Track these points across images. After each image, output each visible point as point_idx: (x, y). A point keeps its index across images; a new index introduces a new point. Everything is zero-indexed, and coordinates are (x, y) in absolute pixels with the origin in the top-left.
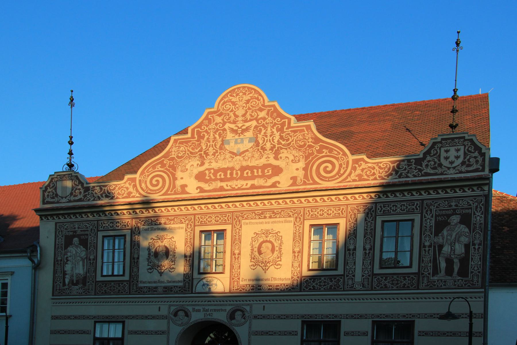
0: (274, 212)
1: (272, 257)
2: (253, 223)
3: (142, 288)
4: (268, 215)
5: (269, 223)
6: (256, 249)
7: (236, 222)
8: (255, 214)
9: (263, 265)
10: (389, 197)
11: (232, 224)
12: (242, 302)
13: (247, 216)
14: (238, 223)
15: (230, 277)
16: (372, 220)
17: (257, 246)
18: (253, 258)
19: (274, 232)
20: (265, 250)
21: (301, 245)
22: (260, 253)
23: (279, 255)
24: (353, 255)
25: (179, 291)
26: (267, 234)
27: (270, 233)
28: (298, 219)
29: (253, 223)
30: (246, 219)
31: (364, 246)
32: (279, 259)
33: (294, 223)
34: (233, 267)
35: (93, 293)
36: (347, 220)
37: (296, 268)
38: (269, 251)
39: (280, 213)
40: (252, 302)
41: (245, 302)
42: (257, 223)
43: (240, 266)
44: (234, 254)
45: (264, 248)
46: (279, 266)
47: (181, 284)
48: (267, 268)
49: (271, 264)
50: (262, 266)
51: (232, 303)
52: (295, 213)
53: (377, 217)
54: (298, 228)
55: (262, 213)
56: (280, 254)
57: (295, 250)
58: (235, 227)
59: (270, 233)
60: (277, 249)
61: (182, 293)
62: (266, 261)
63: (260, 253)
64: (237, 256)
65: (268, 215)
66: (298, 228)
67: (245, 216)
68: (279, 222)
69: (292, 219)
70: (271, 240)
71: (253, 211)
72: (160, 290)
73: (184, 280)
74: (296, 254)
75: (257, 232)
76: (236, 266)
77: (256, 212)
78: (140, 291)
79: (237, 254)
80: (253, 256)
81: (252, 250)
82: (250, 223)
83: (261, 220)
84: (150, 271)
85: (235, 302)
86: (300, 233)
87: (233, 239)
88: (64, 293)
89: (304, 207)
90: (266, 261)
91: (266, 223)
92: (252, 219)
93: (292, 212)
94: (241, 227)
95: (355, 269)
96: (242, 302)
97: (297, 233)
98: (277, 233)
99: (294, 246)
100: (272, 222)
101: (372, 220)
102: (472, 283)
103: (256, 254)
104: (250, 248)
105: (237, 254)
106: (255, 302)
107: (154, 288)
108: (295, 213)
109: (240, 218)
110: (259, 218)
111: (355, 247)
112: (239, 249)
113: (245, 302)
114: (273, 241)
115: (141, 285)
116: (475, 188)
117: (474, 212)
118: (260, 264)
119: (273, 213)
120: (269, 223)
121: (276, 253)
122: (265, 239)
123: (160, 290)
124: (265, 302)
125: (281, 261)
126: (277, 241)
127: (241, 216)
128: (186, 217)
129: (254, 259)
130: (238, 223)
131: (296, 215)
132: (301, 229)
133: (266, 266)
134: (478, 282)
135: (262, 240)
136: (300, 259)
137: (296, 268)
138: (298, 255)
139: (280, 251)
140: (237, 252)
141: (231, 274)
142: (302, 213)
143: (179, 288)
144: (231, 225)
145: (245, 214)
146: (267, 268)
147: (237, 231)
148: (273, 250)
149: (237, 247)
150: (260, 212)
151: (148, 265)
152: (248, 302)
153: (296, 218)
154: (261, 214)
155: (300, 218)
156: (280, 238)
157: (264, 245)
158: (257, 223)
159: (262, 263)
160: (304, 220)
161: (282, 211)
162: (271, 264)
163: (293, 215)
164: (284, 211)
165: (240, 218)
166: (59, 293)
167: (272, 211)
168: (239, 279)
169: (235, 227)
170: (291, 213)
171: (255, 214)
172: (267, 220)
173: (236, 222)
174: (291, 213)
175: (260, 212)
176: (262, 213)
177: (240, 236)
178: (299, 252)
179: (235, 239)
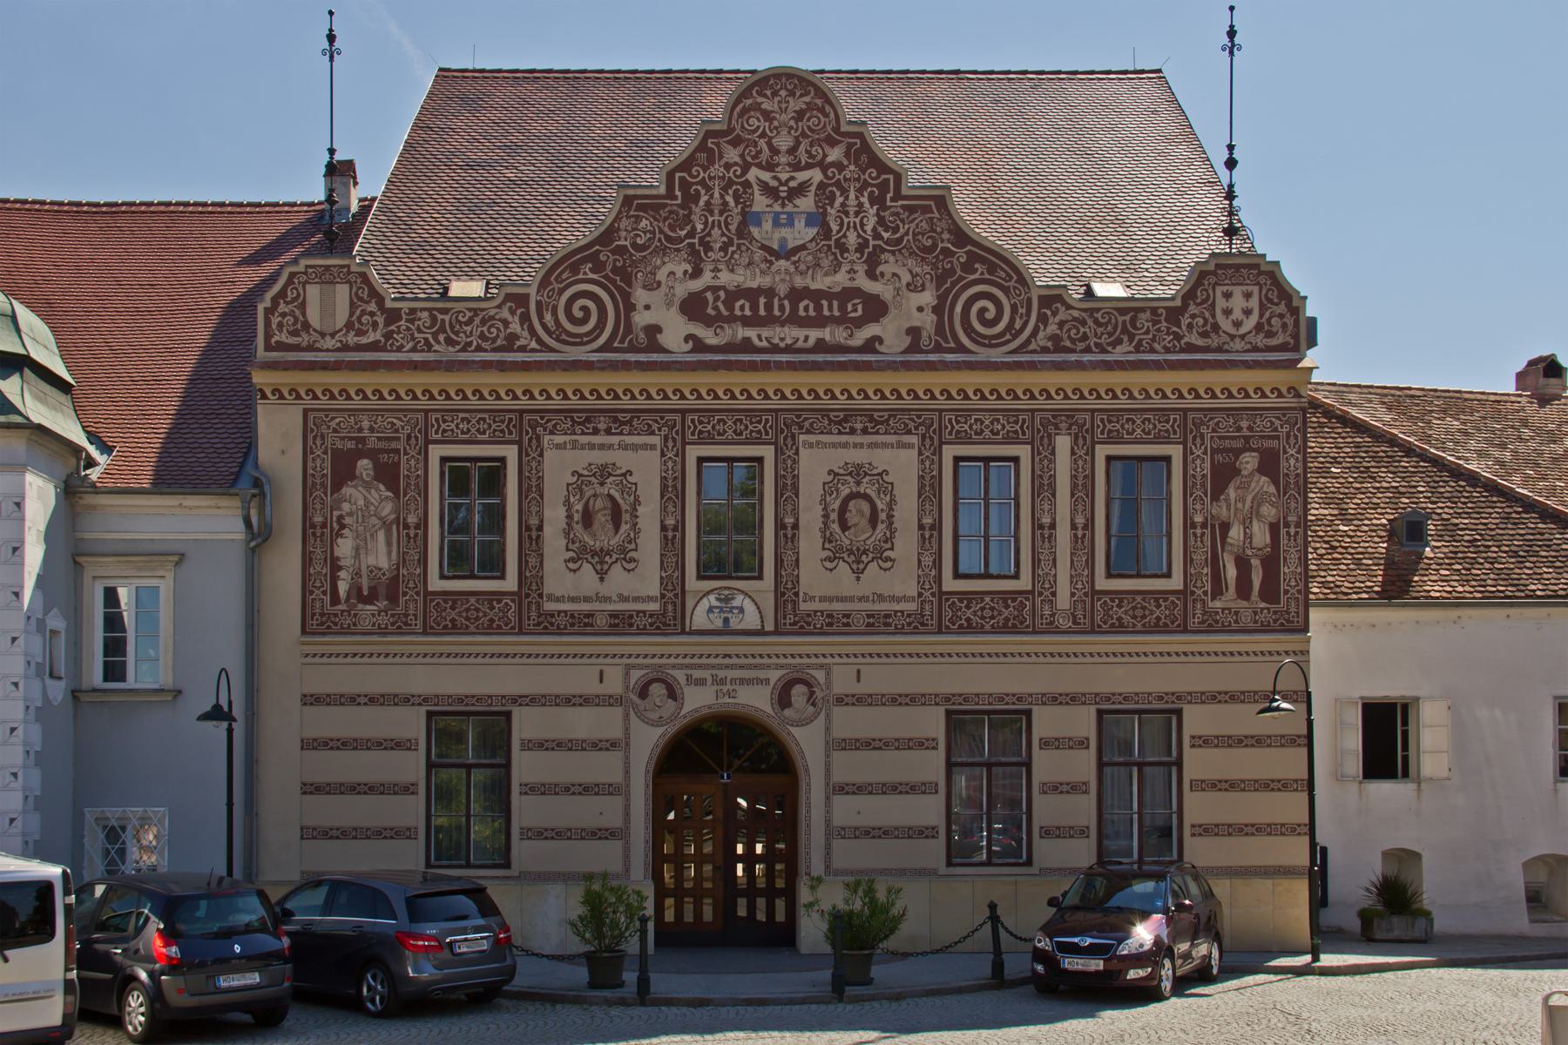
0: (872, 419)
2: (825, 445)
4: (859, 426)
5: (861, 445)
6: (834, 516)
8: (830, 421)
9: (853, 558)
11: (775, 444)
13: (554, 426)
14: (789, 441)
18: (828, 539)
21: (935, 508)
22: (844, 526)
25: (909, 624)
29: (825, 445)
30: (808, 432)
38: (864, 523)
42: (834, 445)
43: (1054, 561)
46: (889, 564)
47: (912, 607)
48: (861, 566)
53: (945, 447)
55: (846, 420)
60: (883, 516)
64: (789, 532)
66: (670, 464)
67: (807, 424)
69: (914, 439)
73: (920, 595)
74: (927, 535)
76: (788, 558)
81: (826, 516)
82: (818, 443)
83: (844, 438)
84: (828, 564)
88: (809, 624)
89: (941, 411)
91: (855, 446)
94: (797, 453)
98: (880, 474)
99: (921, 511)
100: (872, 445)
103: (836, 527)
104: (819, 509)
109: (795, 429)
110: (840, 433)
112: (795, 512)
114: (873, 495)
120: (861, 445)
121: (881, 527)
128: (919, 417)
131: (922, 429)
132: (1089, 466)
135: (847, 491)
136: (935, 546)
138: (416, 535)
139: (891, 523)
140: (789, 520)
142: (936, 426)
143: (651, 616)
146: (861, 566)
147: (534, 464)
148: (873, 521)
149: (790, 508)
150: (841, 414)
152: (821, 660)
153: (666, 438)
155: (674, 440)
157: (852, 504)
158: (834, 445)
159: (851, 552)
166: (795, 623)
168: (796, 594)
170: (911, 425)
172: (858, 439)
173: (785, 438)
175: (841, 414)
176: (846, 420)
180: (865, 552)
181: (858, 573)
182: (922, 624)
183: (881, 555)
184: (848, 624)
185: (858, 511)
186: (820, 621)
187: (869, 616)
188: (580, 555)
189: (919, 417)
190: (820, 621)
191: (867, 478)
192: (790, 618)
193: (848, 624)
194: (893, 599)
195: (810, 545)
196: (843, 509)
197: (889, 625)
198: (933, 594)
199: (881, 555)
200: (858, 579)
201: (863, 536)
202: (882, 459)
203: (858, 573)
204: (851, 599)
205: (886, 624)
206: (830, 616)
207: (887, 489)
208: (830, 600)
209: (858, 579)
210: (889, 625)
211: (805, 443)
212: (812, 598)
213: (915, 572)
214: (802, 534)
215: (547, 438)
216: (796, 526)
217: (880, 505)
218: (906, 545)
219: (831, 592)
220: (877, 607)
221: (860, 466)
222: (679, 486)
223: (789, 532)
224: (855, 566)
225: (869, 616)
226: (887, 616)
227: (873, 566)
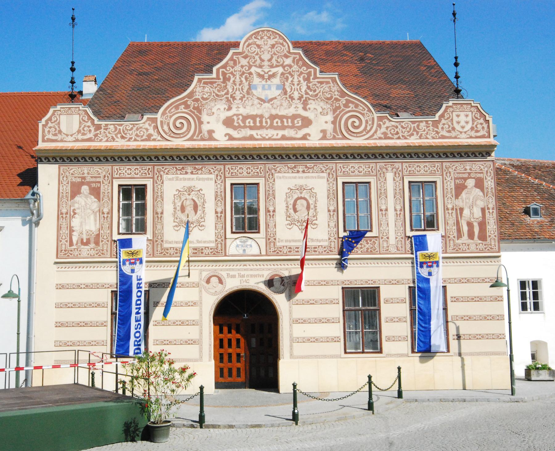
2: (286, 177)
3: (281, 248)
5: (302, 177)
6: (291, 207)
7: (269, 175)
8: (288, 167)
9: (299, 224)
11: (265, 177)
14: (271, 176)
15: (266, 236)
17: (292, 202)
19: (308, 188)
22: (295, 211)
25: (325, 251)
26: (301, 189)
27: (193, 191)
28: (331, 175)
29: (286, 177)
30: (279, 172)
32: (203, 220)
34: (268, 225)
35: (109, 255)
37: (332, 229)
38: (304, 209)
39: (313, 167)
42: (290, 178)
43: (275, 225)
44: (269, 211)
46: (315, 226)
49: (195, 224)
54: (398, 184)
57: (489, 206)
58: (268, 181)
59: (193, 191)
60: (312, 206)
63: (295, 211)
64: (271, 214)
66: (331, 184)
67: (278, 169)
68: (313, 177)
69: (325, 175)
70: (306, 196)
73: (329, 239)
76: (271, 224)
81: (287, 207)
82: (283, 177)
85: (272, 267)
87: (155, 196)
91: (299, 178)
94: (274, 181)
97: (331, 191)
98: (311, 189)
99: (329, 204)
100: (306, 177)
103: (292, 211)
104: (284, 205)
107: (296, 248)
109: (273, 171)
110: (293, 172)
112: (162, 207)
118: (296, 223)
119: (306, 168)
120: (302, 177)
127: (274, 169)
129: (289, 217)
130: (271, 176)
131: (328, 171)
137: (399, 228)
138: (334, 214)
139: (316, 209)
140: (271, 209)
142: (334, 169)
145: (277, 167)
147: (271, 185)
148: (308, 208)
149: (271, 203)
153: (329, 174)
155: (333, 175)
157: (298, 201)
158: (290, 178)
159: (298, 221)
163: (326, 170)
165: (273, 171)
166: (275, 251)
168: (275, 239)
169: (268, 181)
170: (324, 169)
171: (288, 167)
172: (301, 175)
174: (324, 169)
178: (334, 211)
179: (381, 193)
182: (331, 251)
184: (298, 252)
185: (301, 204)
186: (285, 250)
189: (327, 166)
190: (285, 250)
193: (298, 252)
194: (317, 240)
202: (199, 185)
205: (315, 251)
206: (290, 248)
208: (290, 241)
215: (276, 175)
216: (274, 211)
217: (311, 202)
221: (301, 186)
224: (300, 227)
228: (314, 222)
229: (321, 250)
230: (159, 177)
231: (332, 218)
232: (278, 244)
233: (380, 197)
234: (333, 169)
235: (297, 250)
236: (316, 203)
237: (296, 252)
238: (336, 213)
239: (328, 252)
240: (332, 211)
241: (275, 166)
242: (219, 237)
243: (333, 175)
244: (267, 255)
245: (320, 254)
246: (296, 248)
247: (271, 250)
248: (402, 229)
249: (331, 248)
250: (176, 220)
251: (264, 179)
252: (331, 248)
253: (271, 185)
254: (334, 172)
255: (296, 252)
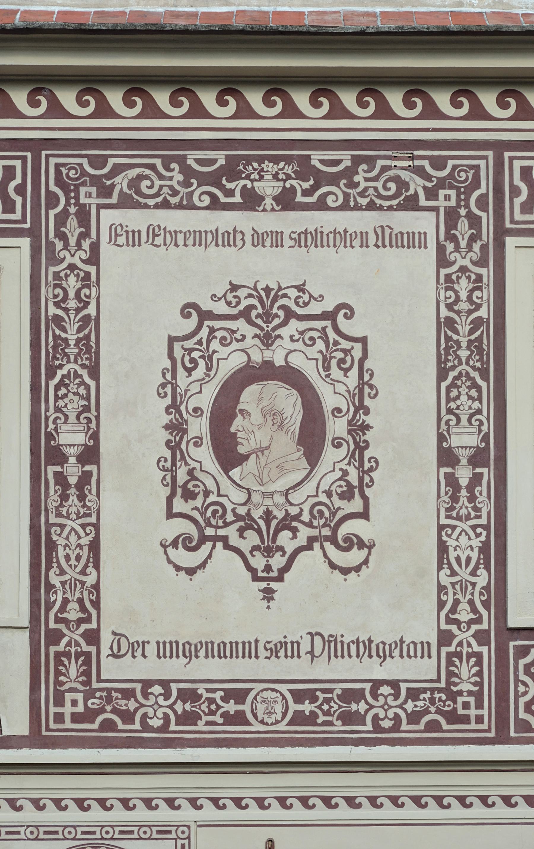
0: (305, 169)
1: (309, 488)
2: (173, 238)
3: (128, 694)
4: (268, 188)
5: (277, 238)
6: (199, 427)
7: (62, 219)
8: (188, 172)
9: (252, 538)
10: (112, 114)
11: (33, 233)
12: (119, 815)
13: (134, 183)
14: (72, 228)
15: (34, 617)
16: (482, 262)
17: (206, 399)
18: (181, 488)
19: (315, 308)
20: (260, 438)
21: (488, 408)
22: (228, 455)
23: (353, 477)
24: (82, 497)
25: (414, 718)
26: (268, 316)
27: (290, 314)
28: (463, 225)
29: (173, 238)
30: (126, 203)
31: (441, 438)
32: (356, 505)
33: (441, 249)
34: (52, 546)
35: (488, 727)
36: (35, 251)
37: (464, 573)
38: (286, 446)
39: (349, 173)
40: (187, 814)
41: (142, 814)
42: (199, 238)
43: (95, 547)
44: (57, 456)
45: (256, 417)
46: (356, 556)
47: (422, 670)
48: (278, 561)
49: (304, 532)
50: (245, 546)
51: (51, 816)
52: (442, 184)
53: (510, 242)
54: (463, 287)
55: (231, 171)
56: (362, 472)
57: (455, 441)
58: (54, 260)
59: (290, 314)
60: (337, 427)
61: (433, 734)
62: (268, 516)
63: (228, 455)
64: (73, 471)
65: (268, 188)
66: (463, 287)
67: (121, 182)
68: (344, 238)
69: (424, 223)
70: (297, 361)
71: (172, 148)
72: (271, 712)
73: (445, 638)
74: (464, 475)
75: (207, 305)
76: (70, 541)
77: (192, 157)
78: (112, 717)
79: (72, 453)
80: (182, 476)
81: (177, 428)
82: (153, 233)
83: (226, 220)
84: (182, 557)
85: (74, 815)
86: (478, 323)
87: (47, 342)
88: (128, 717)
89: (499, 147)
90: (268, 516)
91: (259, 239)
92: (165, 205)
93: (420, 171)
94: (94, 258)
95: (96, 587)
96: (119, 815)
97: (464, 326)
98: (330, 316)
99: (447, 413)
100: (306, 239)
101: (482, 262)
102: (448, 707)
103: (204, 456)
104: (157, 412)
105: (72, 453)
106: (209, 813)
107: (228, 695)
108: (442, 184)
109: (88, 196)
110: (215, 204)
111: (95, 436)
112: (89, 414)
113: (142, 814)
114: (311, 371)
115: (112, 670)
116: (67, 98)
117: (51, 245)
118: (231, 532)
119: (301, 176)
120: (277, 238)
121: (331, 456)
122: (257, 357)
123: (271, 712)
124: (276, 813)
125: (365, 515)
126: (336, 373)
127: (95, 181)
128: (439, 164)
129: (189, 495)
130: (72, 228)
131: (447, 198)
132: (487, 294)
133: (269, 552)
134: (479, 705)
135: (237, 361)
136: (487, 506)
137: (464, 573)
138: (476, 479)
139: (361, 447)
140: (72, 438)
141: (35, 602)
142: (486, 186)
143: (414, 694)
144: (25, 243)
145: (118, 169)
146: (278, 561)
147: (72, 283)
148: (311, 438)
149: (73, 405)
150: (220, 157)
151: (170, 515)
152: (164, 814)
153: (452, 217)
154: (227, 177)
155: (474, 222)
156: (357, 353)
157: (250, 396)
158: (199, 238)
159: (247, 524)
160: (501, 233)
161: (357, 161)
162: (302, 540)
163: (431, 194)
164: (371, 161)
165: (88, 196)
166: (88, 716)
167: (294, 154)
168: (93, 637)
169: (54, 260)
170: (417, 185)
171: (188, 172)
172: (267, 220)
173: (62, 219)
174: (417, 185)
175: (220, 157)
176: (231, 171)
177: (90, 323)
178: (478, 458)
179: (60, 343)
180: (287, 523)
181: (266, 582)
182: (453, 717)
183: (335, 531)
184: (239, 718)
185: (266, 417)
186: (157, 710)
187: (299, 696)
188: (202, 529)
189: (439, 164)
190: (157, 710)
191: (294, 325)
192: (75, 702)
193: (239, 718)
194: (367, 648)
195: (131, 504)
196: (224, 412)
197: (360, 719)
198: (482, 637)
199: (335, 531)
200: (268, 594)
201: (276, 473)
202: (331, 274)
203: (266, 582)
204: (249, 650)
205: (348, 718)
206: (189, 695)
207: (351, 355)
208: (189, 651)
209: (268, 594)
210: (360, 719)
211: (115, 232)
212: (138, 648)
213: (432, 576)
214: (108, 470)
215: (108, 217)
216: (90, 454)
217: (330, 398)
218: (405, 501)
219: (189, 632)
220: (324, 669)
221: (271, 294)
222: (489, 346)
223: (73, 471)
224: (258, 562)
225: (299, 696)
226: (351, 695)
227: (311, 561)
228: (344, 530)
229: (387, 708)
230: (72, 223)
231: (464, 505)
232: (112, 670)
233: (51, 373)
234: (476, 183)
235: (231, 707)
236: (361, 407)
237: (231, 719)
238: (487, 473)
239: (433, 726)
240: (464, 456)
241: (98, 162)
242: (464, 615)
243: (474, 222)
244: (36, 738)
245: (380, 736)
246: (228, 695)
247: (68, 710)
248: (482, 579)
249: (453, 696)
250: (179, 505)
251: (25, 243)
252: (453, 696)
253: (72, 283)
254: (482, 203)
255: (231, 719)
